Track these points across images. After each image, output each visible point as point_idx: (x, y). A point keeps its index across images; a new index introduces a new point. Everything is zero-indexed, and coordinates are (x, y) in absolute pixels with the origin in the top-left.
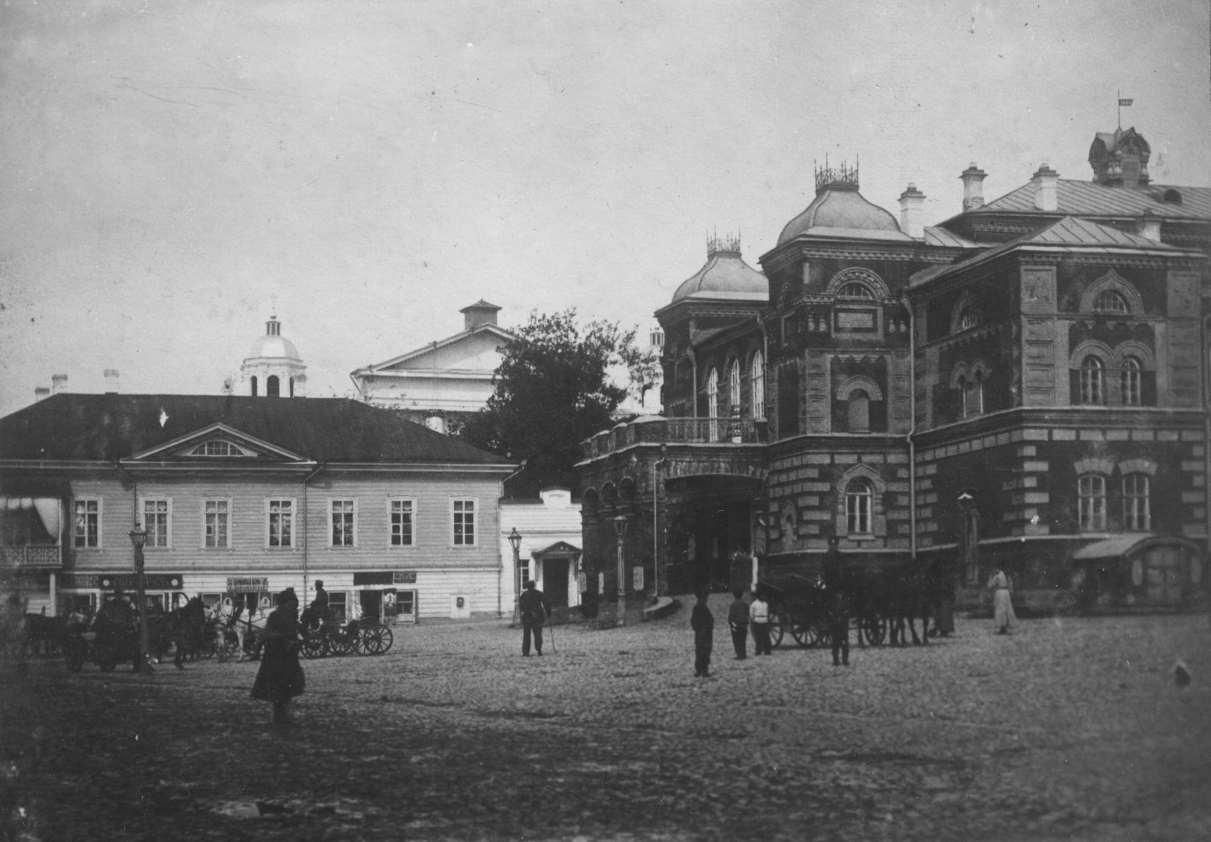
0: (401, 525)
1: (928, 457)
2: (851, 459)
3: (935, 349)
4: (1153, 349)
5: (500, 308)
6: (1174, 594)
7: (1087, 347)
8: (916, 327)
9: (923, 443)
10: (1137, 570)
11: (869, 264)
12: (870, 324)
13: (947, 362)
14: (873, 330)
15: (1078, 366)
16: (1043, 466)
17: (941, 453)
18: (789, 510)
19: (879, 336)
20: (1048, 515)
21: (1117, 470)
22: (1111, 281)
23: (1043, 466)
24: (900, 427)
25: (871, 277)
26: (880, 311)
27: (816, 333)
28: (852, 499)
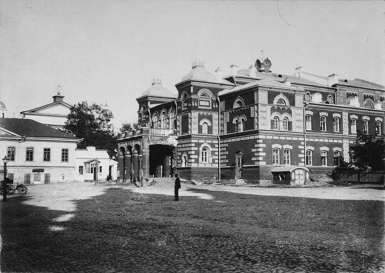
0: (47, 155)
1: (225, 141)
2: (203, 141)
3: (228, 112)
4: (291, 115)
5: (64, 97)
6: (302, 182)
7: (275, 114)
8: (222, 105)
9: (223, 137)
10: (293, 175)
11: (209, 88)
12: (208, 105)
13: (232, 116)
14: (209, 106)
15: (273, 119)
16: (264, 145)
17: (229, 141)
18: (185, 155)
19: (211, 108)
20: (266, 159)
21: (282, 148)
22: (281, 96)
23: (264, 145)
24: (215, 133)
25: (208, 92)
26: (211, 101)
27: (195, 106)
28: (203, 152)
